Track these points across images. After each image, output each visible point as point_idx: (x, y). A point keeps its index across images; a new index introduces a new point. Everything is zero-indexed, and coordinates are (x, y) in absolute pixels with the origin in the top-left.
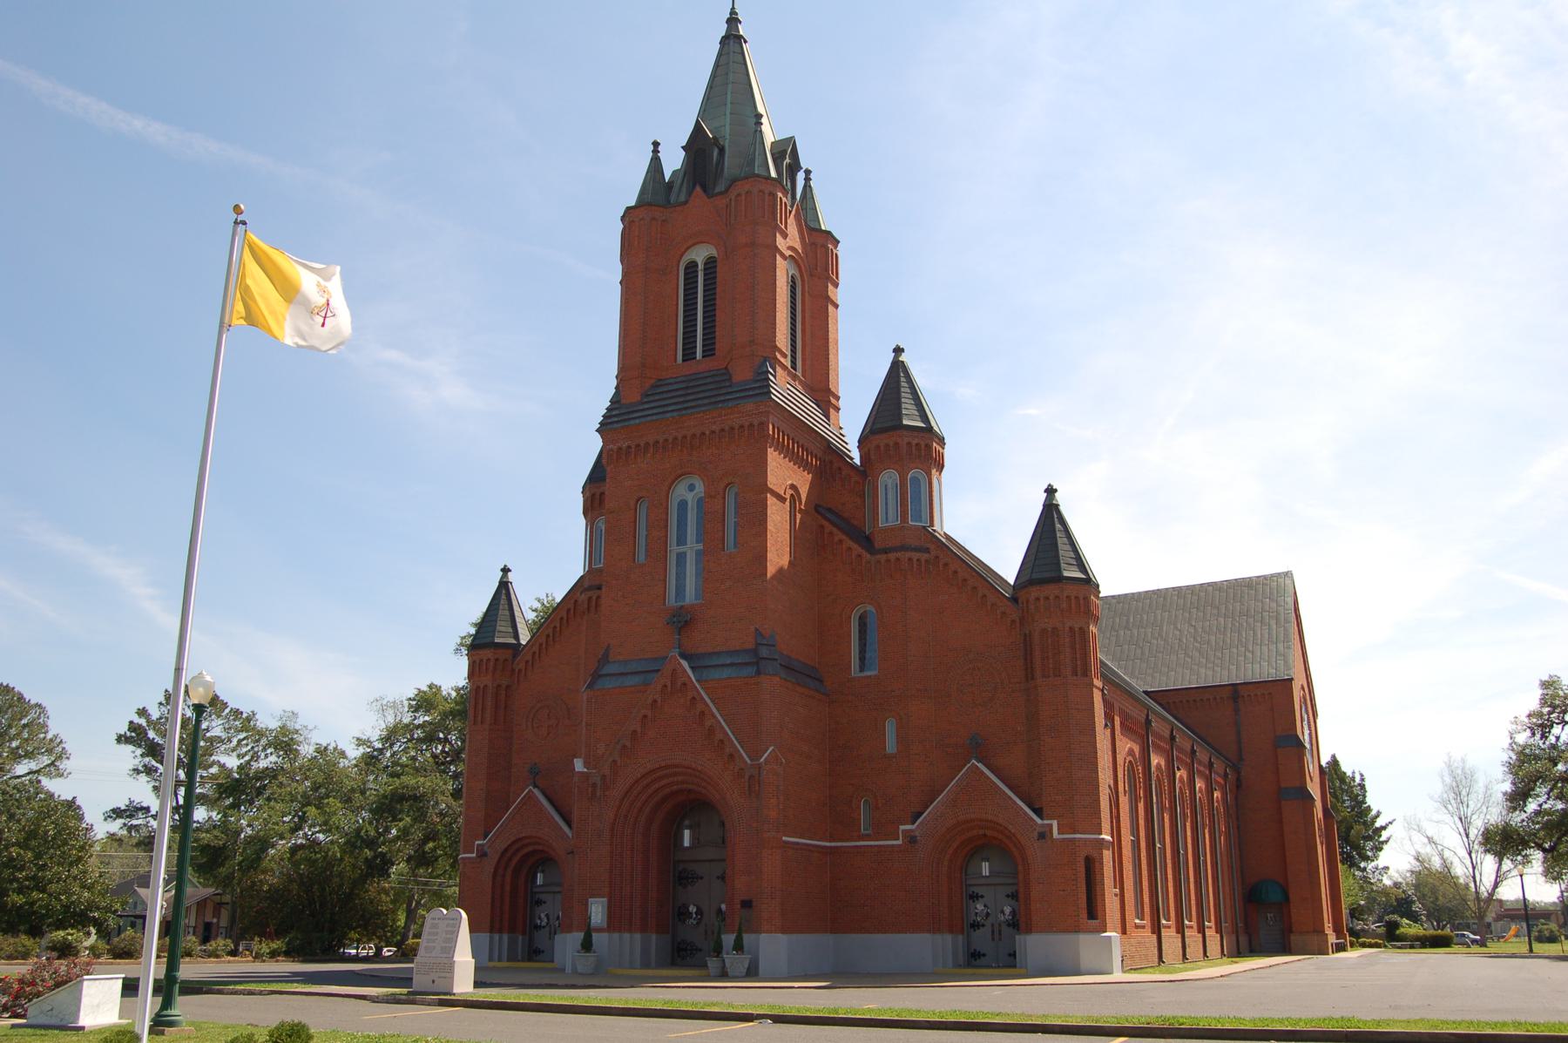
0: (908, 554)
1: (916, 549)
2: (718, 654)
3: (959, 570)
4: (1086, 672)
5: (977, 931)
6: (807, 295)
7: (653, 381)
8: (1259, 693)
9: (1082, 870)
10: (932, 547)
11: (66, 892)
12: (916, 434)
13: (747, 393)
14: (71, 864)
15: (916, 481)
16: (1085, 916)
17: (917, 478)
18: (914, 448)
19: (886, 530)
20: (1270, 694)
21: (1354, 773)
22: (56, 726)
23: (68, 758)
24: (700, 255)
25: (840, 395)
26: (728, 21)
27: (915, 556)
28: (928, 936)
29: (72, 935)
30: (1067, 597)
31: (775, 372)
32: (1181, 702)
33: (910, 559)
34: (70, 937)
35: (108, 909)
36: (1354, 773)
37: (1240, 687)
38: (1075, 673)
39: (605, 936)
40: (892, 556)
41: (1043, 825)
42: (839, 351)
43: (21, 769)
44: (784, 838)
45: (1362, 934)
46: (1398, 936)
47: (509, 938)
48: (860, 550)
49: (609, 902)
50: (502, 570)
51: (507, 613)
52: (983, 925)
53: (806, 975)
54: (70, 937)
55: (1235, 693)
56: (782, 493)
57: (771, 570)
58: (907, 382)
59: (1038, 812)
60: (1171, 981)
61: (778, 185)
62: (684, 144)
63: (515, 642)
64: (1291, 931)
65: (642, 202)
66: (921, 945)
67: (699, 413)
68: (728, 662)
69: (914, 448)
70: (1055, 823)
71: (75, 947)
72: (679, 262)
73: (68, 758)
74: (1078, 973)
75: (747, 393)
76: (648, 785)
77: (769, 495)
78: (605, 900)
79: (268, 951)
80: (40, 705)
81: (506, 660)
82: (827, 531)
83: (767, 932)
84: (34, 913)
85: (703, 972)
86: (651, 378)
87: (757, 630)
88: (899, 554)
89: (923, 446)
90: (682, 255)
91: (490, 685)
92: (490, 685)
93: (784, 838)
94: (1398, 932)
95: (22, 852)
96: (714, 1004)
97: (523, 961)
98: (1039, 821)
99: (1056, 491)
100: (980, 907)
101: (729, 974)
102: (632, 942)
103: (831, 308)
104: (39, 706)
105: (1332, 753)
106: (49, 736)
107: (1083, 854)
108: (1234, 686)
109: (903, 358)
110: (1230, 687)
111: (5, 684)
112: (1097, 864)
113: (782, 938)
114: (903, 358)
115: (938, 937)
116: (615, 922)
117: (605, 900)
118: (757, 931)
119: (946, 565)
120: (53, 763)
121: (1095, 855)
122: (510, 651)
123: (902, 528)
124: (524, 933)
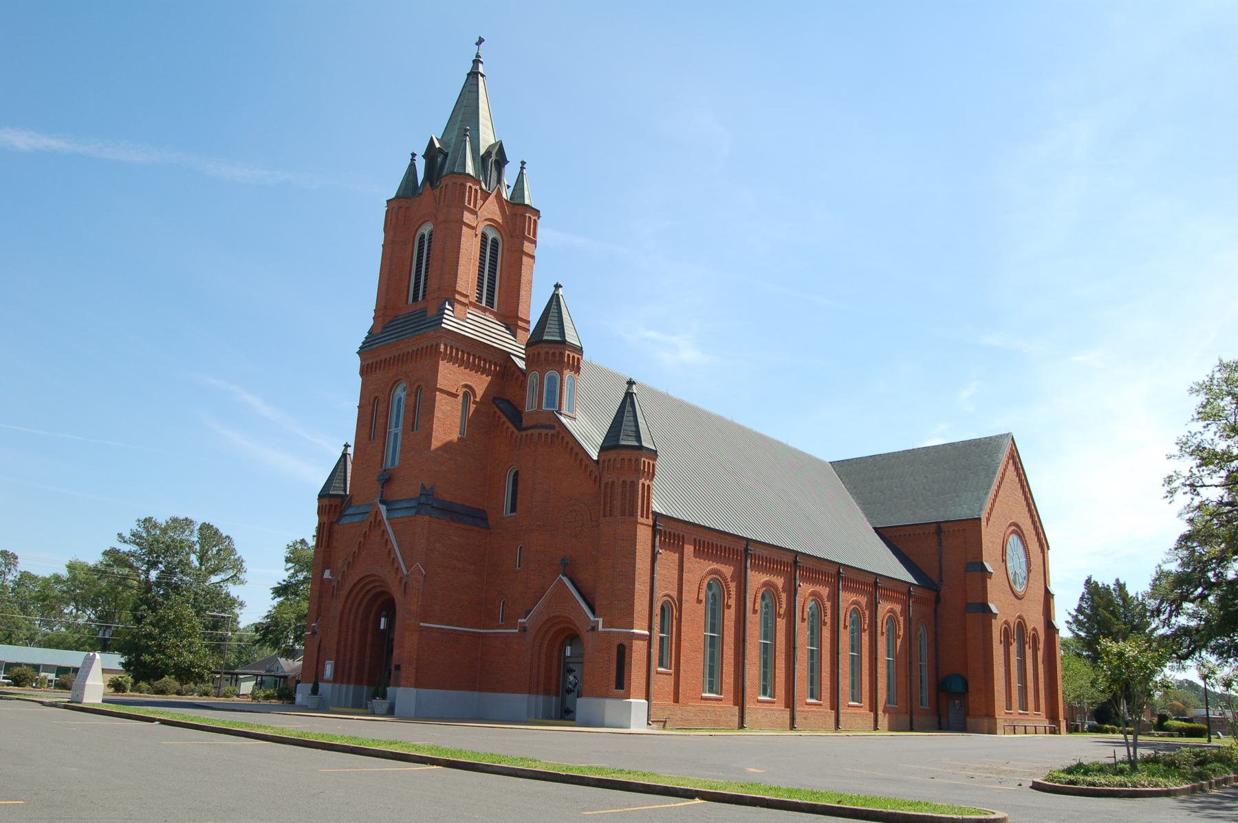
0: (538, 431)
1: (543, 427)
2: (401, 500)
3: (570, 441)
4: (633, 513)
5: (570, 695)
6: (505, 250)
7: (391, 318)
8: (956, 529)
9: (615, 654)
10: (556, 425)
11: (180, 654)
12: (552, 345)
13: (430, 324)
14: (184, 637)
15: (552, 379)
16: (614, 686)
17: (552, 376)
18: (550, 356)
19: (531, 414)
20: (964, 530)
21: (1137, 594)
22: (241, 550)
23: (245, 572)
24: (426, 229)
25: (530, 319)
26: (474, 61)
27: (544, 432)
28: (525, 696)
29: (123, 677)
30: (622, 459)
31: (453, 308)
32: (900, 536)
33: (540, 434)
34: (120, 679)
35: (206, 667)
36: (1137, 594)
37: (942, 525)
38: (623, 513)
39: (330, 685)
40: (529, 432)
41: (594, 622)
42: (533, 289)
43: (214, 579)
44: (421, 624)
45: (1130, 723)
46: (1165, 726)
47: (43, 672)
48: (514, 429)
49: (335, 663)
50: (345, 445)
51: (342, 474)
52: (573, 691)
53: (442, 717)
54: (120, 679)
55: (939, 529)
56: (454, 392)
57: (435, 444)
58: (557, 305)
59: (593, 611)
60: (630, 734)
61: (468, 177)
62: (423, 154)
63: (343, 493)
64: (967, 714)
65: (397, 197)
66: (520, 700)
67: (406, 339)
68: (405, 506)
69: (550, 356)
70: (601, 620)
71: (123, 686)
72: (415, 235)
73: (245, 572)
74: (602, 726)
75: (430, 324)
76: (362, 588)
77: (437, 393)
78: (333, 662)
79: (263, 695)
80: (229, 537)
81: (336, 506)
82: (497, 415)
83: (405, 686)
84: (158, 668)
85: (364, 711)
86: (390, 316)
87: (422, 484)
88: (533, 431)
89: (557, 354)
90: (417, 231)
91: (326, 522)
92: (326, 522)
93: (421, 624)
94: (1165, 724)
95: (153, 629)
96: (259, 727)
97: (542, 719)
98: (592, 618)
99: (631, 379)
100: (571, 678)
101: (376, 712)
102: (348, 690)
103: (525, 259)
104: (228, 537)
105: (1116, 578)
106: (236, 557)
107: (617, 642)
108: (938, 524)
109: (561, 291)
110: (935, 525)
111: (207, 523)
112: (627, 650)
113: (413, 690)
114: (561, 291)
115: (533, 697)
116: (337, 678)
117: (333, 662)
118: (397, 685)
119: (563, 438)
120: (235, 575)
121: (626, 643)
122: (339, 500)
123: (537, 412)
124: (557, 695)
